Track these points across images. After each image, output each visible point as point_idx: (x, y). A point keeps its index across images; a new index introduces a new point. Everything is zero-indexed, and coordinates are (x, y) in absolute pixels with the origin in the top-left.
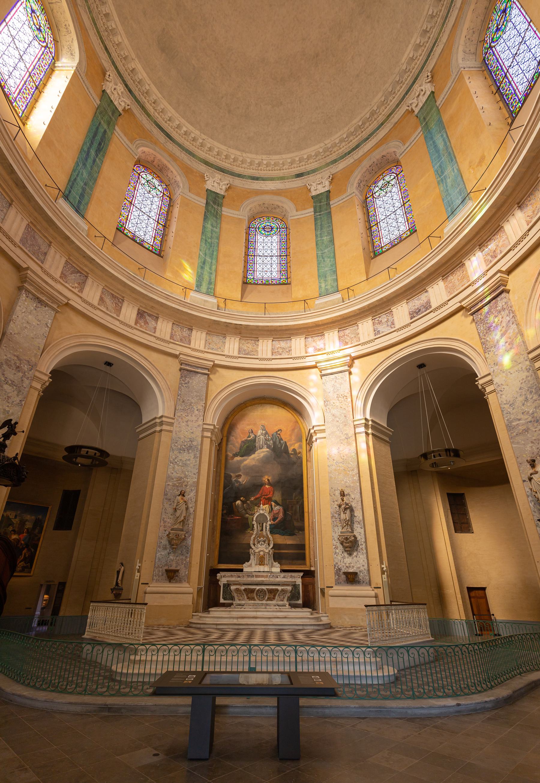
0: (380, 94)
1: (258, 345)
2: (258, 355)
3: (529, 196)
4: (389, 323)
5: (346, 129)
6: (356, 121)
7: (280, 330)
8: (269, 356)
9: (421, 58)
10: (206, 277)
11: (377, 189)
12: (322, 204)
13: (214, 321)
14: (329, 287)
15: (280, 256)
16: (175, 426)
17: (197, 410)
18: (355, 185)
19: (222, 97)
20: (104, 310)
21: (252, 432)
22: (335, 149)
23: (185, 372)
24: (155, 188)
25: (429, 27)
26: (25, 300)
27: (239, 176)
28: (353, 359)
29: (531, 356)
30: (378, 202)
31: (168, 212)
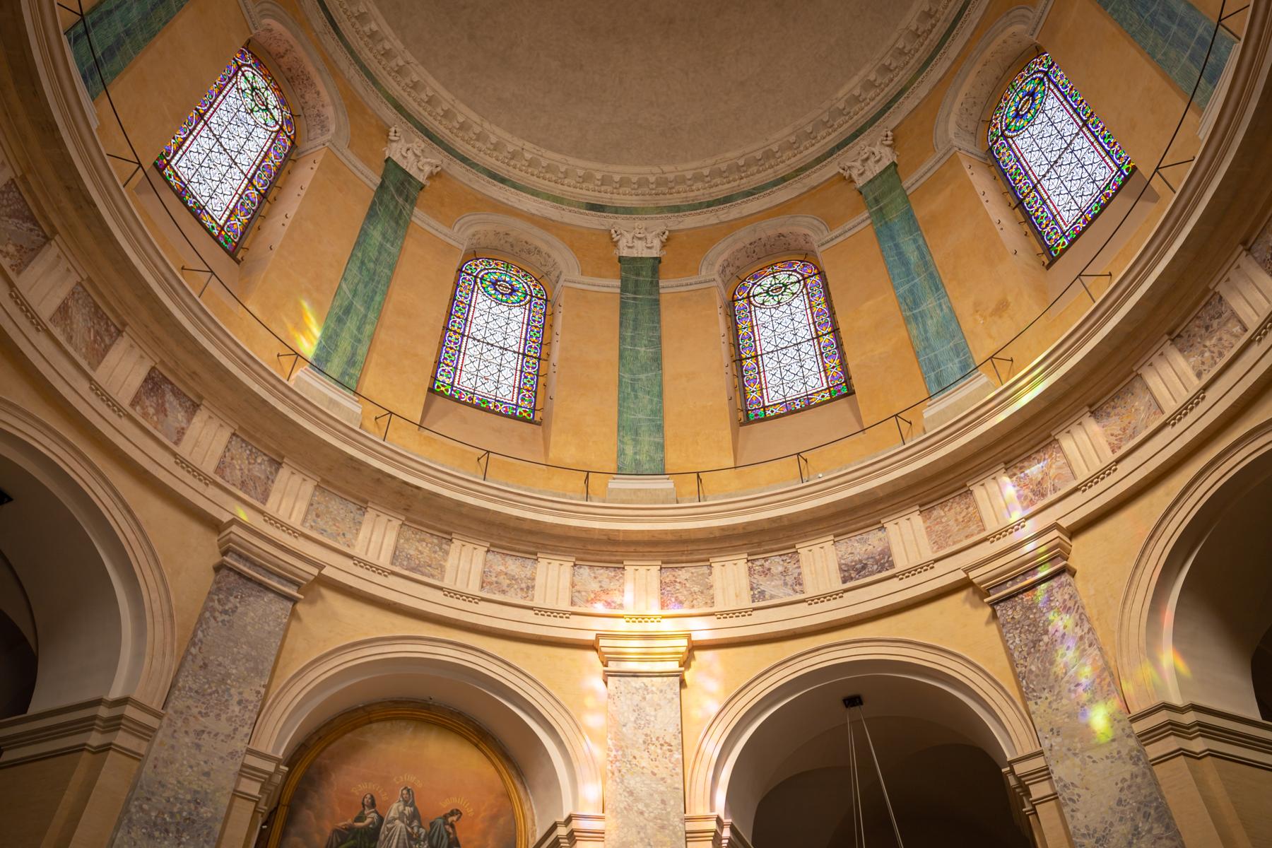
0: (786, 131)
1: (447, 553)
2: (442, 579)
3: (1117, 396)
4: (790, 580)
5: (713, 160)
6: (732, 155)
7: (515, 529)
8: (474, 589)
9: (872, 104)
10: (345, 344)
11: (759, 290)
12: (640, 280)
13: (352, 458)
14: (643, 457)
15: (524, 354)
16: (158, 740)
17: (240, 703)
18: (717, 267)
19: (464, 7)
20: (62, 339)
21: (373, 805)
22: (681, 188)
23: (233, 578)
24: (267, 109)
25: (894, 65)
27: (464, 160)
28: (695, 647)
29: (1139, 727)
30: (761, 316)
31: (279, 169)
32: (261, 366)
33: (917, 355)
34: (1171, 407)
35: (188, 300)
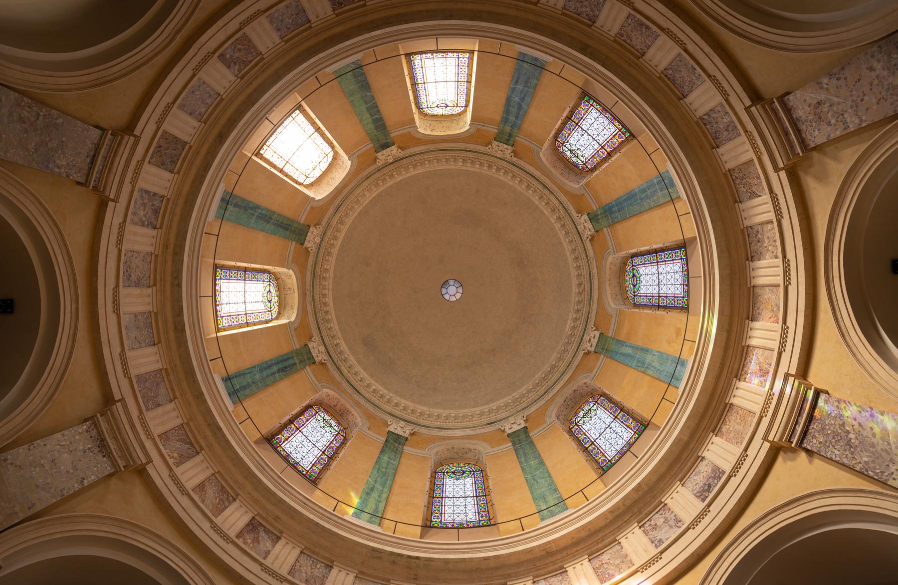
3: (754, 307)
4: (672, 523)
12: (521, 441)
13: (374, 550)
18: (554, 415)
26: (80, 434)
32: (317, 505)
33: (658, 379)
34: (780, 280)
35: (271, 473)
